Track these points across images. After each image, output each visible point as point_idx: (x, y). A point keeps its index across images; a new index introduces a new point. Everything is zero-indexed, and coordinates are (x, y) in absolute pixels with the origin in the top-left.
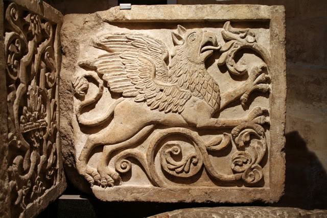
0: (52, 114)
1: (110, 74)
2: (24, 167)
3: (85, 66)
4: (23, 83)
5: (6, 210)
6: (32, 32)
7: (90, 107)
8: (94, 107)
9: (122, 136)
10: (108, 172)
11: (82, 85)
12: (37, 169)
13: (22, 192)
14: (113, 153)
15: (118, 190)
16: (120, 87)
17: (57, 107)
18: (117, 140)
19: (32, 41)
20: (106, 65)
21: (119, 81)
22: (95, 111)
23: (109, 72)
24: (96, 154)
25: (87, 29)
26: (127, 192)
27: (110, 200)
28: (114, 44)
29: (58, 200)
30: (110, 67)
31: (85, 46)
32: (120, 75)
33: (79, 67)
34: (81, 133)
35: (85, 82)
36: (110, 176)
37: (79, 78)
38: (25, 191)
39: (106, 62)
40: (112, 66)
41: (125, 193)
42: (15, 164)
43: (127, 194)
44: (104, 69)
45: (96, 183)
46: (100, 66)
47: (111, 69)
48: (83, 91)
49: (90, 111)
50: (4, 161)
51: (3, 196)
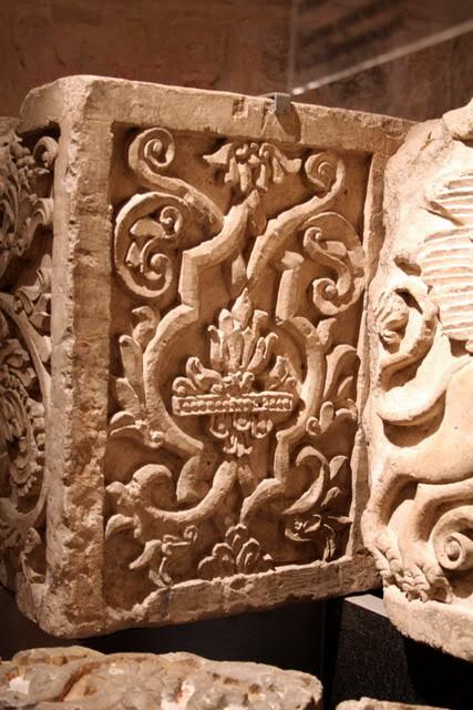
0: (329, 382)
1: (445, 287)
2: (177, 493)
3: (405, 265)
4: (187, 304)
5: (86, 570)
6: (239, 184)
7: (402, 373)
8: (412, 376)
9: (453, 464)
10: (417, 558)
11: (388, 314)
12: (241, 507)
13: (158, 548)
14: (437, 508)
15: (432, 614)
16: (463, 324)
17: (361, 367)
18: (444, 474)
19: (241, 206)
20: (439, 261)
21: (460, 308)
22: (414, 385)
23: (443, 281)
24: (406, 501)
25: (424, 162)
26: (451, 627)
27: (415, 636)
28: (461, 202)
29: (336, 604)
30: (446, 267)
31: (411, 209)
32: (465, 290)
33: (393, 265)
34: (386, 439)
35: (396, 305)
36: (421, 568)
37: (385, 296)
38: (170, 547)
39: (438, 253)
40: (452, 265)
41: (447, 627)
42: (136, 481)
43: (450, 633)
44: (433, 271)
45: (393, 581)
46: (428, 264)
47: (447, 272)
48: (392, 330)
49: (407, 384)
50: (89, 468)
51: (74, 538)
